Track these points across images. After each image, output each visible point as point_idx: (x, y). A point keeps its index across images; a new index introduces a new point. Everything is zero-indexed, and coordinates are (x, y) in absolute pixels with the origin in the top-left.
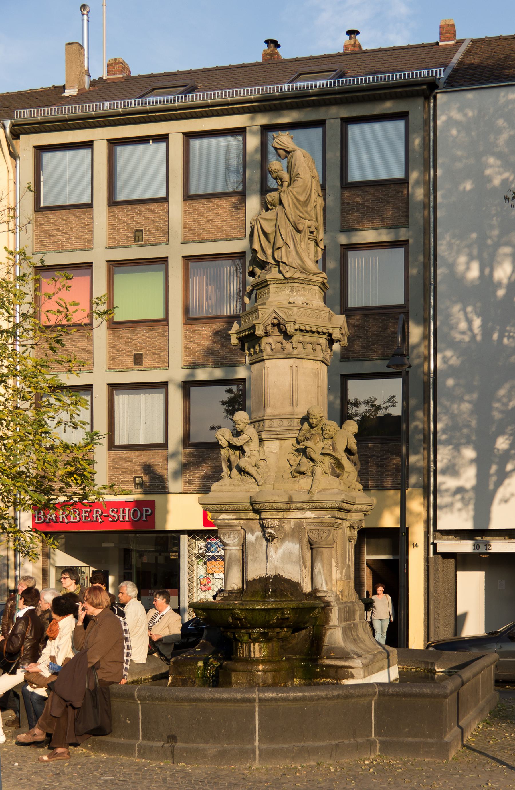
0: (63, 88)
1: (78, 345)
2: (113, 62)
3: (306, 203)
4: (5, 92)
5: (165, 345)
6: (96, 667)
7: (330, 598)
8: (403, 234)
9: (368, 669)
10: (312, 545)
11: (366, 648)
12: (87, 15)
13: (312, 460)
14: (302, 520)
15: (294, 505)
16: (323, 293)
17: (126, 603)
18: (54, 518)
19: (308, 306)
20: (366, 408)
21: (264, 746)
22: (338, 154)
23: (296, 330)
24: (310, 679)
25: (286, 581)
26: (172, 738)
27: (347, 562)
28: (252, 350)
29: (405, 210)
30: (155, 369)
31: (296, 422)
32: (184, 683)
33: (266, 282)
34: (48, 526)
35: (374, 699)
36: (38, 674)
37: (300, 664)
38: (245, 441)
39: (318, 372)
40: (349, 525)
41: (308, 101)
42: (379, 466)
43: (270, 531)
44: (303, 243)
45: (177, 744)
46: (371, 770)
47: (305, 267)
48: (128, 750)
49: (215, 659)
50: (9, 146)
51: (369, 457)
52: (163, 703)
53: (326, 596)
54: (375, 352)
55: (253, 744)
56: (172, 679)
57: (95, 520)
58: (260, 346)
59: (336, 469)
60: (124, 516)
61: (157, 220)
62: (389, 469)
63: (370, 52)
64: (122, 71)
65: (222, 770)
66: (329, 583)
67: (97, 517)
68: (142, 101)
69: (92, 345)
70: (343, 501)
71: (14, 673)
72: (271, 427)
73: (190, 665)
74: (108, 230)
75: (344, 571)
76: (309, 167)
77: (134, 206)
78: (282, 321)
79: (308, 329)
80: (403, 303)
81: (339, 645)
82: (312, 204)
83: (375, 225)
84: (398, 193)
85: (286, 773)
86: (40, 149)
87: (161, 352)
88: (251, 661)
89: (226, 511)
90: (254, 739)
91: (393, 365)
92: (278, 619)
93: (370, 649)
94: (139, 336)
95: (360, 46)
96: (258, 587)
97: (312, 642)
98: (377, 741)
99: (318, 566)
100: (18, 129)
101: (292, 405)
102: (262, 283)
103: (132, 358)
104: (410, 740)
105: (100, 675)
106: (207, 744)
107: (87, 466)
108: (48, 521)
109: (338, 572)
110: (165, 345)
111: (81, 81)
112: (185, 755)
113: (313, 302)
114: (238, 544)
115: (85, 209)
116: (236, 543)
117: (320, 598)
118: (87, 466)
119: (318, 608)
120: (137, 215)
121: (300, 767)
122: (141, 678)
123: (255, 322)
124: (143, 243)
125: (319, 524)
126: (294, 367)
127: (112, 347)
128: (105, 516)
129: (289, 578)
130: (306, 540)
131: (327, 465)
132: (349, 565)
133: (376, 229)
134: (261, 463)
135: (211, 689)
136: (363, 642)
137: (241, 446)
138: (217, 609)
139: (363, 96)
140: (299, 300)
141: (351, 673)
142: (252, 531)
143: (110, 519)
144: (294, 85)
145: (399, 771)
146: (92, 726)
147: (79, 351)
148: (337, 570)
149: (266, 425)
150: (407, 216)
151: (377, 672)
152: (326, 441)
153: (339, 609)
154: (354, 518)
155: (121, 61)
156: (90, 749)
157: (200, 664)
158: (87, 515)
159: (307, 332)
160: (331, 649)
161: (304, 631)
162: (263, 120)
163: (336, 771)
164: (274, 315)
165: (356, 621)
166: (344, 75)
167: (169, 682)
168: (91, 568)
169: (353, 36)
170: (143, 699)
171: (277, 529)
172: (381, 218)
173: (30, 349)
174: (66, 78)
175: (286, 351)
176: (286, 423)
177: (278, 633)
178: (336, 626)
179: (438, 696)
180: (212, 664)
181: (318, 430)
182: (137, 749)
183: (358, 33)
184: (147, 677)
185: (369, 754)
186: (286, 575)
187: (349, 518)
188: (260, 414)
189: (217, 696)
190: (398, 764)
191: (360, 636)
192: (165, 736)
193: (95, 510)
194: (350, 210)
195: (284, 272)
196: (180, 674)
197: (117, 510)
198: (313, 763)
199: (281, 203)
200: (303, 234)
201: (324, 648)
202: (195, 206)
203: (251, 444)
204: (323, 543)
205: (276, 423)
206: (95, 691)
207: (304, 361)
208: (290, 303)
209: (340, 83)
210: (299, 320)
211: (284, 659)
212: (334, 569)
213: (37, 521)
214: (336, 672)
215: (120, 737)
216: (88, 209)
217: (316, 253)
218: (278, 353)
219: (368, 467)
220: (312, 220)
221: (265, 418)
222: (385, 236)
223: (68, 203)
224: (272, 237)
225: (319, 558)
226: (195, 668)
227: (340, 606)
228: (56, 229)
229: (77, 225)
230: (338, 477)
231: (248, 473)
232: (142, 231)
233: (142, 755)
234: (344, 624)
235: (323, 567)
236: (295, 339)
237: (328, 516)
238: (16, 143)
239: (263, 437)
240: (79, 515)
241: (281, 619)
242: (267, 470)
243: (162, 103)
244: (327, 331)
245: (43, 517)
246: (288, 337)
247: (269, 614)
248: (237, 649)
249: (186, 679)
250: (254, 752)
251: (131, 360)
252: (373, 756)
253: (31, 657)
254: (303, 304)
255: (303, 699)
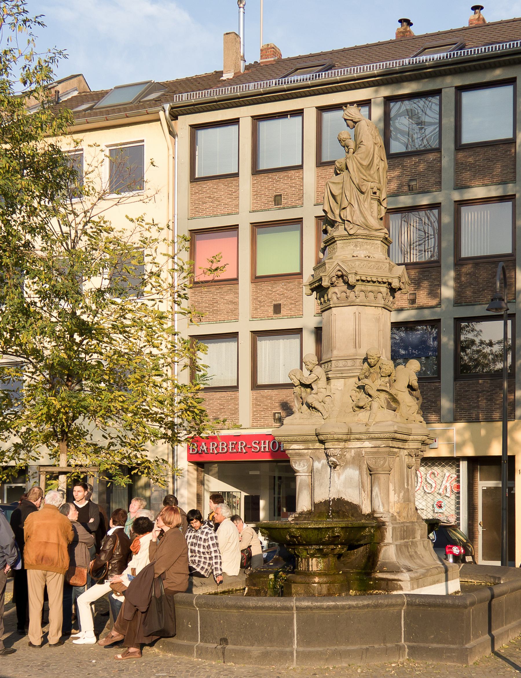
0: (220, 73)
1: (226, 298)
2: (266, 47)
3: (369, 166)
4: (175, 79)
5: (300, 296)
6: (162, 577)
7: (386, 519)
8: (510, 189)
9: (417, 581)
10: (371, 471)
11: (422, 563)
12: (244, 8)
13: (370, 396)
14: (361, 449)
15: (353, 436)
16: (387, 247)
17: (221, 523)
18: (205, 450)
19: (370, 259)
20: (500, 348)
21: (301, 649)
22: (453, 119)
23: (358, 281)
24: (365, 590)
25: (347, 503)
26: (224, 641)
27: (406, 487)
28: (322, 299)
29: (513, 167)
30: (291, 317)
31: (359, 362)
32: (258, 593)
33: (334, 238)
34: (200, 456)
35: (404, 608)
36: (120, 583)
37: (356, 577)
38: (313, 380)
39: (379, 317)
40: (407, 454)
41: (425, 73)
42: (489, 400)
43: (332, 459)
44: (366, 203)
45: (228, 646)
46: (393, 672)
47: (368, 224)
48: (188, 650)
49: (284, 572)
50: (169, 127)
51: (480, 392)
52: (217, 610)
53: (382, 517)
54: (485, 297)
55: (292, 647)
56: (248, 590)
57: (240, 451)
58: (327, 295)
59: (392, 403)
60: (265, 447)
61: (294, 185)
62: (498, 402)
63: (493, 25)
64: (273, 54)
65: (262, 669)
66: (386, 505)
67: (241, 448)
68: (285, 80)
69: (237, 297)
70: (396, 432)
71: (102, 582)
72: (337, 367)
73: (263, 577)
74: (252, 196)
75: (402, 494)
76: (372, 135)
77: (274, 174)
78: (344, 273)
79: (369, 279)
80: (511, 252)
81: (392, 560)
82: (374, 168)
83: (486, 182)
84: (506, 152)
85: (317, 673)
86: (195, 128)
87: (297, 302)
88: (309, 574)
89: (296, 442)
90: (292, 642)
91: (492, 309)
92: (329, 537)
93: (427, 564)
94: (278, 288)
95: (484, 20)
96: (323, 509)
97: (369, 558)
98: (406, 646)
99: (376, 490)
100: (176, 111)
101: (356, 348)
102: (330, 240)
103: (272, 308)
104: (435, 645)
105: (166, 584)
106: (253, 646)
107: (196, 404)
108: (200, 452)
109: (396, 495)
110: (300, 296)
111: (237, 66)
112: (233, 655)
113: (375, 256)
114: (308, 470)
115: (233, 179)
116: (306, 470)
117: (376, 518)
118: (196, 404)
119: (368, 527)
120: (277, 181)
121: (331, 668)
122: (233, 589)
123: (321, 275)
124: (281, 206)
125: (376, 453)
126: (357, 313)
127: (255, 299)
128: (249, 448)
129: (350, 501)
130: (365, 467)
131: (383, 401)
132: (408, 489)
133: (486, 185)
134: (327, 399)
135: (255, 598)
136: (421, 558)
137: (310, 384)
138: (276, 528)
139: (474, 66)
140: (362, 253)
141: (400, 585)
142: (319, 459)
143: (253, 450)
144: (418, 58)
145: (417, 673)
146: (156, 628)
147: (227, 303)
148: (395, 494)
149: (333, 366)
150: (515, 172)
151: (430, 585)
152: (383, 379)
153: (394, 529)
154: (410, 447)
155: (273, 46)
156: (161, 649)
157: (271, 576)
158: (233, 446)
159: (369, 282)
160: (384, 564)
161: (362, 547)
162: (386, 92)
163: (362, 672)
164: (338, 268)
165: (416, 539)
166: (464, 47)
167: (245, 593)
168: (242, 492)
169: (477, 11)
170: (200, 606)
171: (339, 458)
172: (491, 175)
173: (158, 303)
174: (224, 64)
175: (349, 300)
176: (350, 363)
177: (332, 549)
178: (390, 544)
179: (459, 606)
180: (281, 577)
181: (377, 368)
182: (195, 650)
183: (482, 8)
184: (238, 588)
185: (397, 658)
186: (347, 498)
187: (407, 447)
188: (329, 356)
189: (260, 604)
190: (421, 667)
191: (419, 553)
192: (218, 638)
193: (240, 443)
194: (463, 169)
195: (348, 229)
196: (254, 585)
197: (259, 442)
198: (345, 665)
199: (347, 168)
200: (366, 194)
201: (379, 563)
202: (327, 171)
203: (319, 382)
204: (380, 469)
205: (341, 363)
206: (161, 598)
207: (366, 307)
208: (353, 256)
209: (462, 54)
210: (360, 271)
211: (341, 572)
212: (392, 493)
213: (191, 452)
214: (387, 584)
215: (183, 639)
216: (235, 178)
217: (379, 211)
218: (343, 302)
219: (479, 401)
220: (374, 182)
221: (332, 359)
222: (494, 191)
223: (218, 174)
224: (339, 199)
225: (376, 483)
226: (267, 581)
227: (395, 526)
228: (208, 197)
229: (226, 192)
230: (395, 411)
231: (315, 408)
232: (281, 195)
233: (199, 656)
234: (399, 542)
235: (380, 491)
236: (357, 289)
237: (383, 446)
238: (175, 123)
239: (330, 376)
240: (226, 447)
241: (332, 537)
242: (332, 405)
243: (299, 81)
244: (387, 281)
245: (226, 448)
246: (351, 287)
247: (321, 533)
248: (298, 563)
249: (259, 590)
250: (292, 653)
251: (271, 310)
252: (401, 660)
253: (119, 570)
254: (366, 257)
255: (336, 607)
